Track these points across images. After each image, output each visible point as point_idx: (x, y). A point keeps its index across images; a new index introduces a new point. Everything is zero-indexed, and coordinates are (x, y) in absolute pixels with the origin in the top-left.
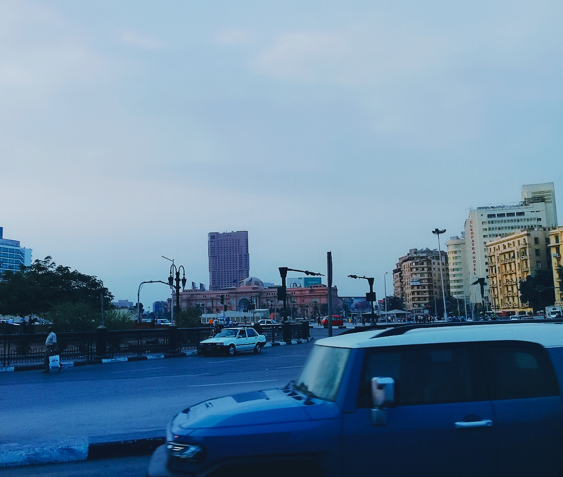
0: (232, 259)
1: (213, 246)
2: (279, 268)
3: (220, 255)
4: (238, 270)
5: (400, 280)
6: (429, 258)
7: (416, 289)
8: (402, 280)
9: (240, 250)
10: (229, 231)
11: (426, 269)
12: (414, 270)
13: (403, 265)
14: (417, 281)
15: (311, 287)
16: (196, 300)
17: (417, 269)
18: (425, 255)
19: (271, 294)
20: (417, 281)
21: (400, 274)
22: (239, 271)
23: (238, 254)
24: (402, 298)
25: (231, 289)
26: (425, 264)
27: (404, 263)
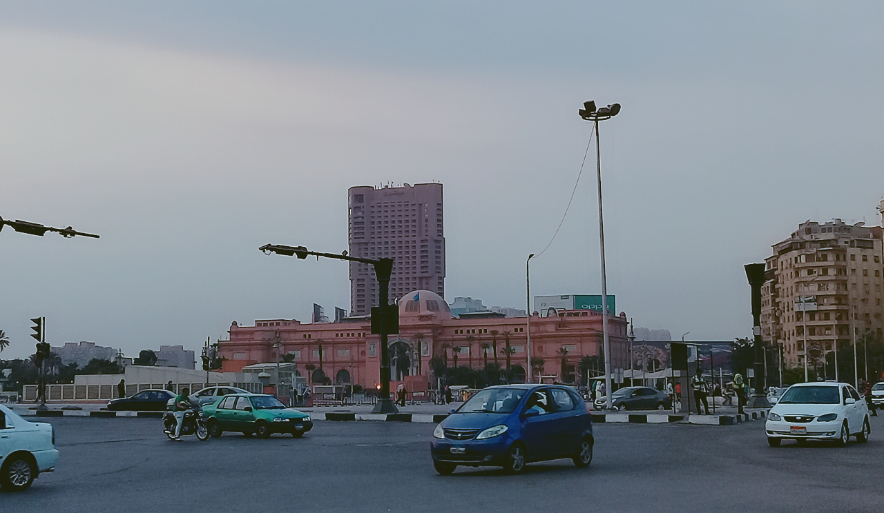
2: (747, 268)
3: (376, 241)
4: (418, 275)
5: (774, 298)
6: (841, 243)
7: (806, 322)
8: (777, 300)
9: (424, 228)
10: (398, 184)
11: (832, 272)
12: (804, 273)
13: (780, 260)
14: (810, 301)
15: (562, 315)
17: (810, 272)
18: (831, 236)
19: (345, 335)
20: (810, 301)
21: (773, 284)
22: (421, 278)
23: (417, 239)
24: (775, 342)
26: (831, 257)
27: (783, 258)
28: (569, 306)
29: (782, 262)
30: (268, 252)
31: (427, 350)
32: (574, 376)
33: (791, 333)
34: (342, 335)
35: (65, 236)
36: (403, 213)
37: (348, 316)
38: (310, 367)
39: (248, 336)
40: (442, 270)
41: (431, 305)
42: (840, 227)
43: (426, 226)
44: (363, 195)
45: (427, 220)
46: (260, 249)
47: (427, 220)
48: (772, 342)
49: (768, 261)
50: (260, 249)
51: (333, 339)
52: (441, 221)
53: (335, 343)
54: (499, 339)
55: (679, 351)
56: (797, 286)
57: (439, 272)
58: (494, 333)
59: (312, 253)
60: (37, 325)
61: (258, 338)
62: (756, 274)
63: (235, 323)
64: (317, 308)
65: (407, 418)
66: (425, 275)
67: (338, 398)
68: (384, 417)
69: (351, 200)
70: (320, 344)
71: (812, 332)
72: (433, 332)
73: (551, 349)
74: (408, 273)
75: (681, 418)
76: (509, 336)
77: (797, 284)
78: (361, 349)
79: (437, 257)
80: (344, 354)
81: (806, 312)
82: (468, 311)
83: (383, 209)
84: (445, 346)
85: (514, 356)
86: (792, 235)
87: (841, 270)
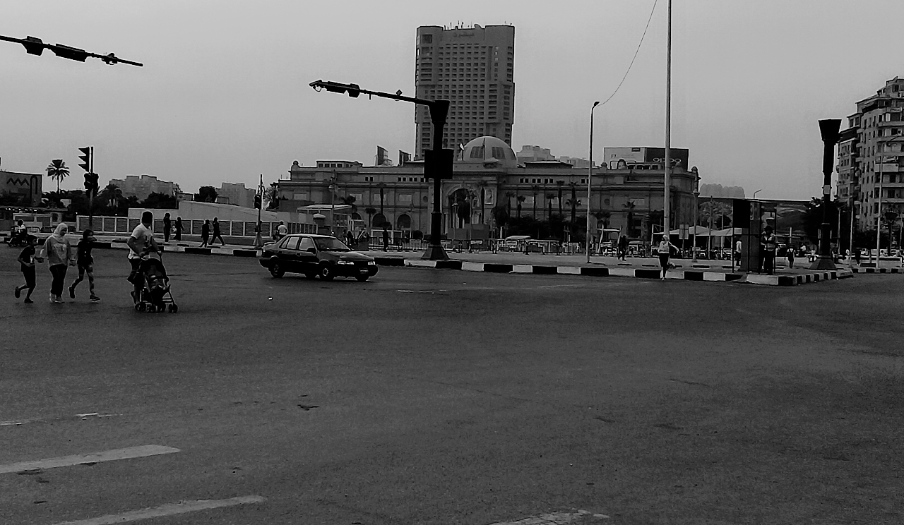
1: (428, 61)
2: (823, 123)
3: (444, 83)
4: (486, 120)
7: (886, 182)
9: (493, 72)
10: (468, 24)
12: (887, 133)
13: (863, 118)
14: (891, 162)
15: (631, 168)
16: (347, 187)
17: (895, 131)
19: (407, 180)
20: (891, 162)
21: (855, 143)
23: (486, 84)
24: (852, 203)
27: (866, 116)
28: (640, 158)
29: (866, 121)
30: (318, 88)
31: (491, 198)
32: (640, 230)
33: (869, 194)
34: (404, 179)
35: (108, 63)
36: (458, 56)
37: (412, 160)
38: (370, 210)
39: (310, 177)
40: (510, 117)
41: (497, 152)
44: (431, 36)
45: (496, 64)
46: (310, 85)
48: (848, 203)
49: (851, 118)
50: (310, 85)
51: (395, 183)
53: (396, 188)
54: (565, 189)
55: (742, 210)
56: (879, 147)
57: (508, 119)
58: (560, 183)
59: (365, 92)
60: (85, 155)
61: (319, 179)
62: (829, 129)
63: (296, 163)
64: (381, 151)
65: (457, 265)
66: (492, 121)
67: (396, 243)
68: (434, 264)
69: (419, 41)
70: (382, 188)
71: (891, 195)
72: (498, 180)
73: (618, 202)
74: (461, 118)
75: (739, 277)
76: (575, 187)
77: (879, 144)
78: (424, 194)
79: (505, 103)
80: (405, 199)
81: (884, 173)
82: (535, 159)
83: (451, 51)
84: (509, 195)
85: (579, 208)
86: (878, 92)
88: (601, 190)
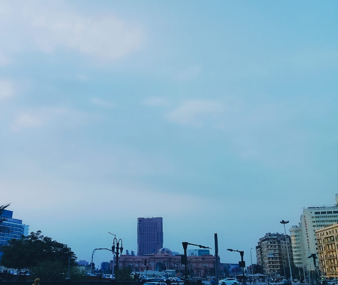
0: (148, 235)
1: (141, 227)
4: (156, 242)
6: (279, 239)
8: (262, 254)
9: (157, 229)
11: (277, 247)
13: (262, 243)
15: (203, 256)
16: (128, 262)
17: (271, 247)
18: (276, 237)
21: (261, 249)
22: (157, 243)
24: (262, 265)
25: (151, 255)
26: (276, 243)
27: (263, 242)
33: (267, 263)
36: (150, 225)
42: (278, 235)
43: (158, 229)
45: (158, 227)
47: (158, 227)
52: (162, 227)
56: (268, 250)
71: (273, 263)
78: (149, 264)
87: (279, 246)
88: (196, 262)
